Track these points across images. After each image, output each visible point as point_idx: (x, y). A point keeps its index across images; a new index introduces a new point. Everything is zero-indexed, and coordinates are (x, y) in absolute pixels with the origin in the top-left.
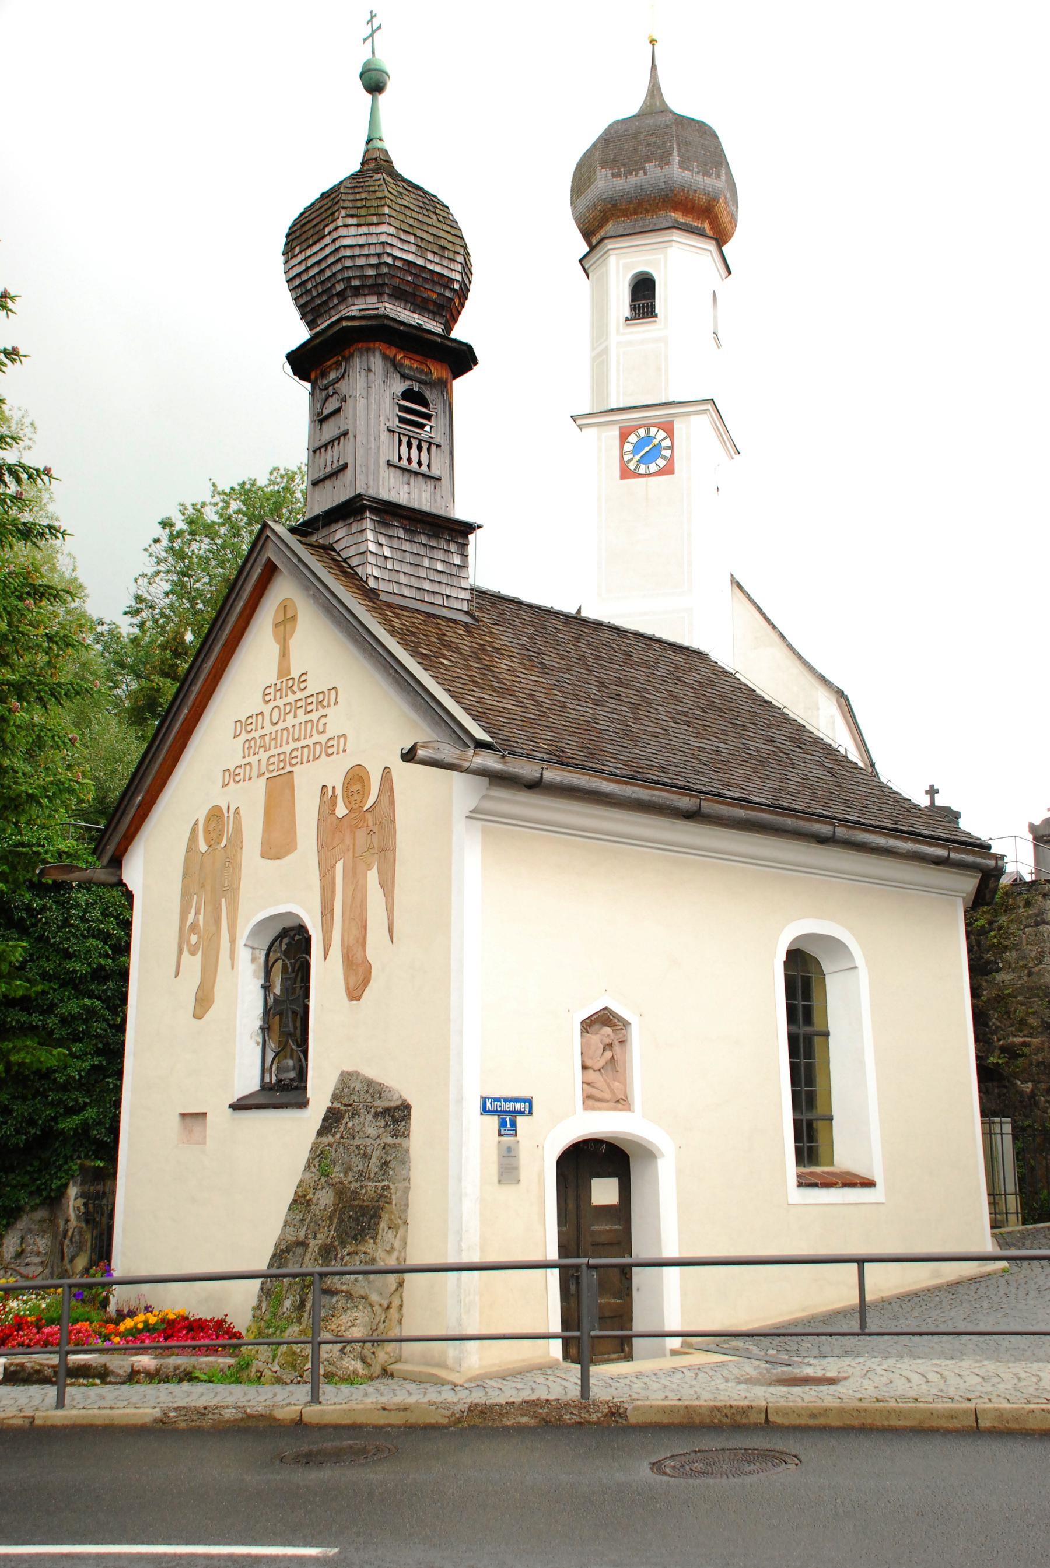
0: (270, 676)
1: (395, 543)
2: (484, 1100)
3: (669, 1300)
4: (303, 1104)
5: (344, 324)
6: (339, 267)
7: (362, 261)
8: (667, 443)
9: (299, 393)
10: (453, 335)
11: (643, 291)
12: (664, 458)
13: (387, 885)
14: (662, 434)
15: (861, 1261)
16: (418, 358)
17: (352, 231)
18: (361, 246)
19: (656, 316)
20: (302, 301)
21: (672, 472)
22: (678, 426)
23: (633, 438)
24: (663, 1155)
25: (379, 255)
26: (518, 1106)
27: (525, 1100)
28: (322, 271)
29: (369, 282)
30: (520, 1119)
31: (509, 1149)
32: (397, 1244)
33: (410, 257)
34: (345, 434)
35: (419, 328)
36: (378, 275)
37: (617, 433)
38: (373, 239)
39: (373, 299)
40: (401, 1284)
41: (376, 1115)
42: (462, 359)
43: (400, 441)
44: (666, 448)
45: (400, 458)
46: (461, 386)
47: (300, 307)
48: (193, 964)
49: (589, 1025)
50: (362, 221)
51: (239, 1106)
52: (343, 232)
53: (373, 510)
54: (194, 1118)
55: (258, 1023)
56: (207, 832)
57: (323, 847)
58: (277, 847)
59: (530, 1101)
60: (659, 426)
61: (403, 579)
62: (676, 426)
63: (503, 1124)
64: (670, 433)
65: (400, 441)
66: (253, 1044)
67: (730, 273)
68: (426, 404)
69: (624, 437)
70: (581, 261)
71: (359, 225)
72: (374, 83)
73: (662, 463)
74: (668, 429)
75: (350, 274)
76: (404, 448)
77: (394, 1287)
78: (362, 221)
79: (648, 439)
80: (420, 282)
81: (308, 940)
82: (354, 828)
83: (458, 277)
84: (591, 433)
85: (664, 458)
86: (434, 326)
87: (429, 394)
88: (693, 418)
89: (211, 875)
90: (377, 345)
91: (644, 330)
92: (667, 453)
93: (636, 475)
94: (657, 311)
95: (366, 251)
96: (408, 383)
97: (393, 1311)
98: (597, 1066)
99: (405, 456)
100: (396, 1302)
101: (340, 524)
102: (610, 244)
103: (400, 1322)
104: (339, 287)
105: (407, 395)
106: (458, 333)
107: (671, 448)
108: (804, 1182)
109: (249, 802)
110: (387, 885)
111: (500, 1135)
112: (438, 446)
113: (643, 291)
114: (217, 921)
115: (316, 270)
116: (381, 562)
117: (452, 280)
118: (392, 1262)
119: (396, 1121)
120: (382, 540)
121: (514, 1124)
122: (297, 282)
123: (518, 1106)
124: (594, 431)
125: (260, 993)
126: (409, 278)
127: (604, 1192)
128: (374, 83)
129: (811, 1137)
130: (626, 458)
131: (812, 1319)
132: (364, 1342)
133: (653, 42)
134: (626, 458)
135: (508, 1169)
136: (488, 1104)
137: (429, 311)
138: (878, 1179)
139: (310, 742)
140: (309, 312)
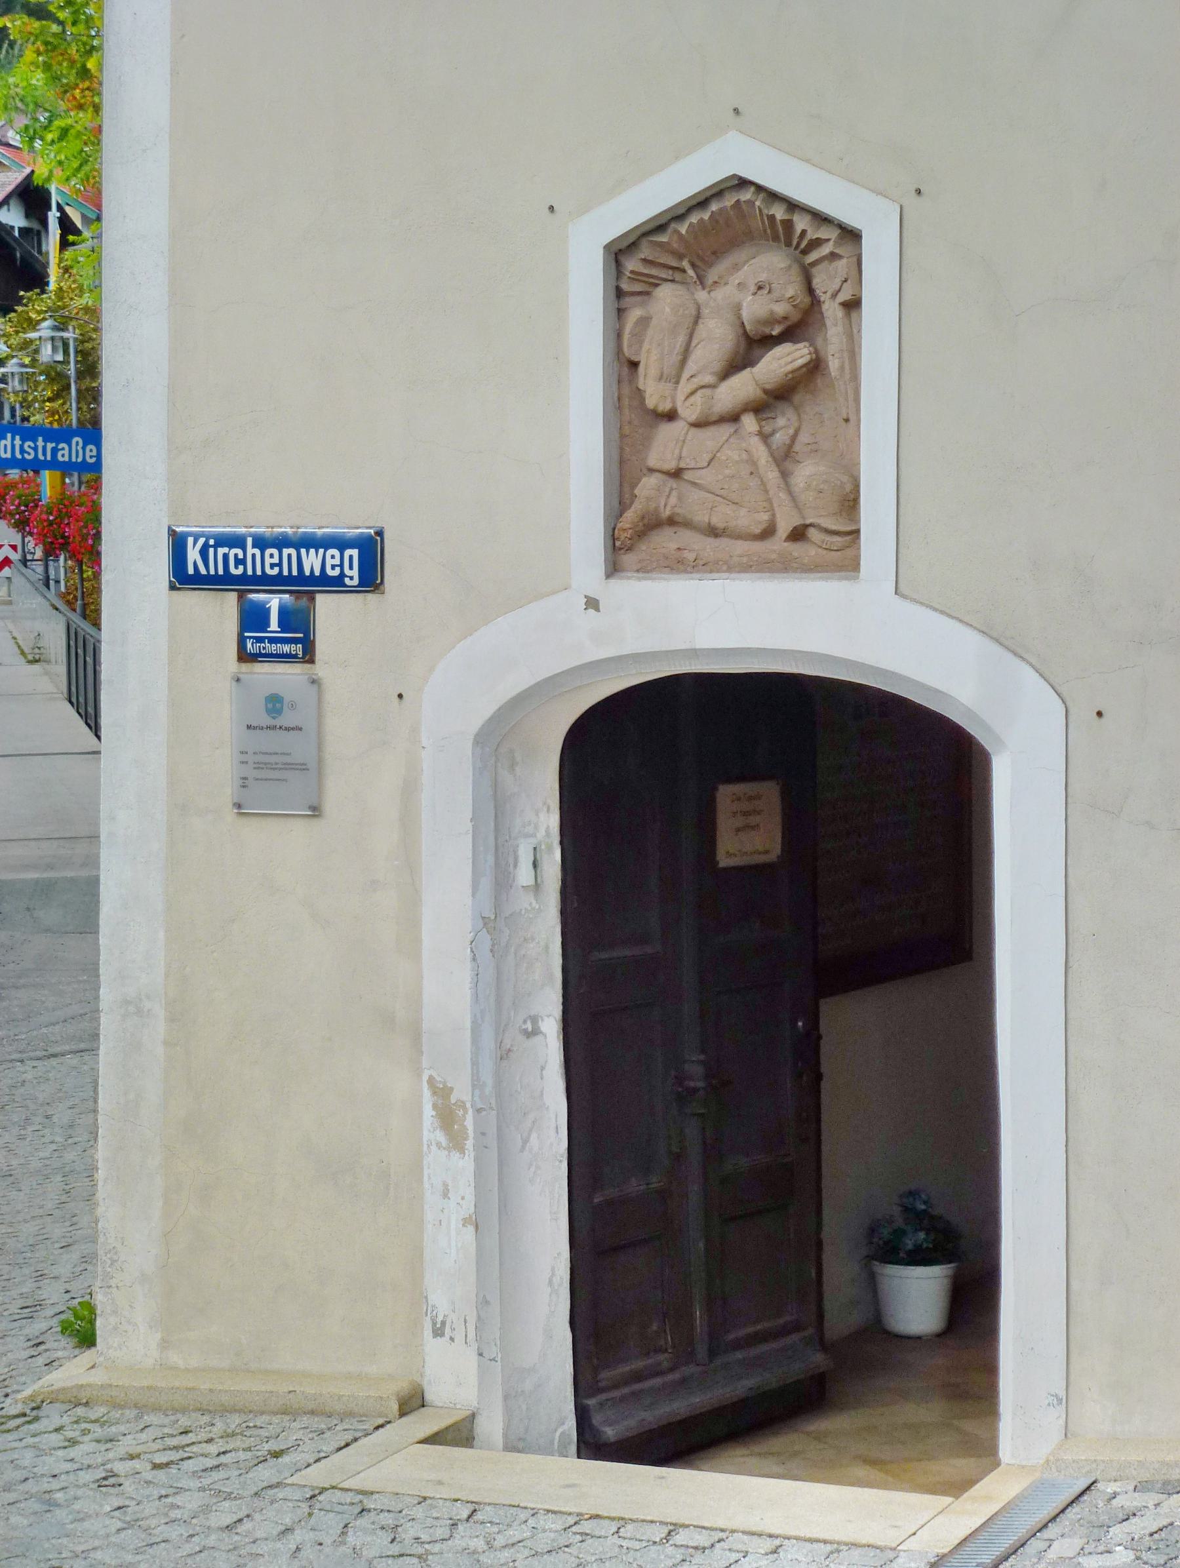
2: (178, 544)
26: (312, 561)
27: (341, 544)
63: (253, 618)
121: (299, 625)
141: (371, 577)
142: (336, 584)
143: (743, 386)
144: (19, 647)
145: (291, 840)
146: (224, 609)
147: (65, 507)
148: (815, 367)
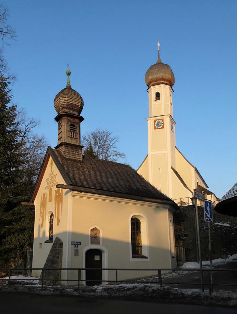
0: (50, 172)
1: (69, 150)
2: (72, 242)
3: (106, 275)
4: (52, 242)
5: (61, 114)
6: (60, 104)
7: (64, 104)
8: (162, 123)
9: (56, 124)
10: (81, 115)
11: (158, 95)
14: (161, 121)
15: (117, 270)
16: (74, 119)
17: (62, 99)
19: (160, 100)
21: (163, 128)
22: (164, 120)
23: (156, 122)
24: (104, 252)
30: (79, 245)
31: (76, 250)
32: (60, 265)
33: (71, 102)
34: (62, 132)
37: (154, 121)
40: (61, 272)
41: (59, 244)
42: (82, 119)
43: (70, 133)
45: (70, 136)
46: (82, 124)
47: (56, 111)
48: (41, 218)
50: (63, 97)
51: (46, 242)
52: (60, 99)
53: (65, 144)
54: (41, 244)
56: (43, 197)
57: (55, 200)
59: (81, 243)
60: (161, 120)
62: (164, 119)
63: (75, 246)
65: (70, 133)
67: (173, 91)
68: (75, 126)
70: (147, 90)
73: (162, 126)
74: (162, 120)
75: (62, 106)
76: (71, 134)
77: (59, 272)
78: (63, 97)
79: (159, 122)
83: (80, 105)
86: (76, 113)
89: (43, 205)
90: (62, 118)
91: (158, 102)
92: (162, 125)
93: (157, 129)
94: (160, 99)
96: (71, 123)
99: (73, 136)
100: (60, 274)
101: (61, 147)
102: (152, 87)
104: (61, 108)
106: (81, 115)
107: (163, 123)
108: (133, 257)
111: (75, 248)
112: (77, 133)
113: (158, 95)
114: (44, 212)
115: (57, 105)
118: (59, 268)
119: (61, 245)
120: (66, 149)
121: (77, 246)
122: (56, 107)
123: (78, 243)
125: (49, 224)
127: (97, 258)
132: (54, 280)
135: (76, 253)
136: (73, 243)
137: (75, 111)
138: (149, 257)
139: (54, 183)
140: (58, 111)
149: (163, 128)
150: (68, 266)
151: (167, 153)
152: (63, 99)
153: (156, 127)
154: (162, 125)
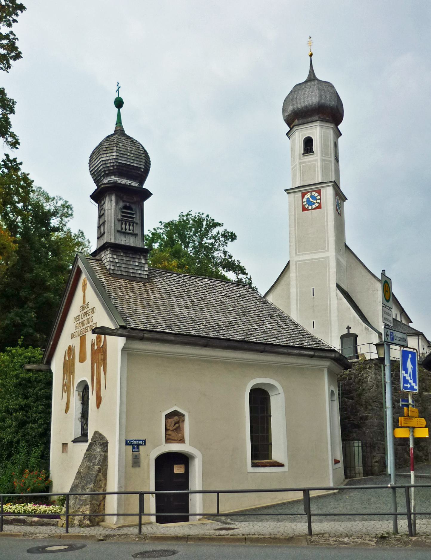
2: (127, 441)
7: (108, 165)
8: (319, 197)
11: (308, 144)
12: (308, 207)
13: (105, 371)
17: (105, 155)
18: (108, 160)
20: (95, 178)
23: (317, 194)
25: (113, 163)
26: (140, 442)
27: (142, 441)
28: (98, 169)
29: (111, 171)
32: (103, 485)
35: (130, 185)
36: (114, 169)
37: (301, 195)
38: (111, 158)
39: (113, 177)
42: (147, 194)
44: (318, 199)
45: (122, 229)
47: (94, 180)
48: (65, 395)
49: (168, 416)
55: (80, 415)
58: (82, 359)
59: (145, 441)
60: (316, 191)
61: (123, 269)
63: (134, 448)
64: (320, 194)
66: (79, 422)
69: (303, 196)
70: (287, 134)
71: (107, 153)
72: (119, 103)
73: (317, 205)
74: (319, 192)
77: (102, 498)
80: (128, 170)
81: (88, 388)
82: (99, 353)
84: (292, 195)
85: (308, 207)
86: (135, 184)
87: (133, 207)
88: (328, 188)
91: (309, 158)
92: (319, 201)
95: (109, 162)
97: (102, 506)
98: (171, 429)
103: (104, 509)
105: (125, 207)
106: (145, 186)
107: (320, 199)
109: (76, 343)
110: (105, 371)
113: (308, 144)
115: (96, 168)
116: (114, 264)
117: (141, 168)
120: (115, 257)
121: (138, 448)
123: (140, 442)
124: (292, 195)
126: (125, 169)
127: (178, 469)
128: (119, 103)
129: (261, 451)
130: (304, 204)
131: (254, 509)
133: (311, 55)
134: (304, 204)
141: (145, 444)
142: (141, 445)
143: (175, 427)
144: (84, 292)
145: (137, 469)
146: (131, 447)
147: (388, 301)
148: (179, 426)
149: (319, 207)
150: (120, 487)
151: (328, 257)
152: (108, 155)
153: (306, 207)
154: (317, 203)
